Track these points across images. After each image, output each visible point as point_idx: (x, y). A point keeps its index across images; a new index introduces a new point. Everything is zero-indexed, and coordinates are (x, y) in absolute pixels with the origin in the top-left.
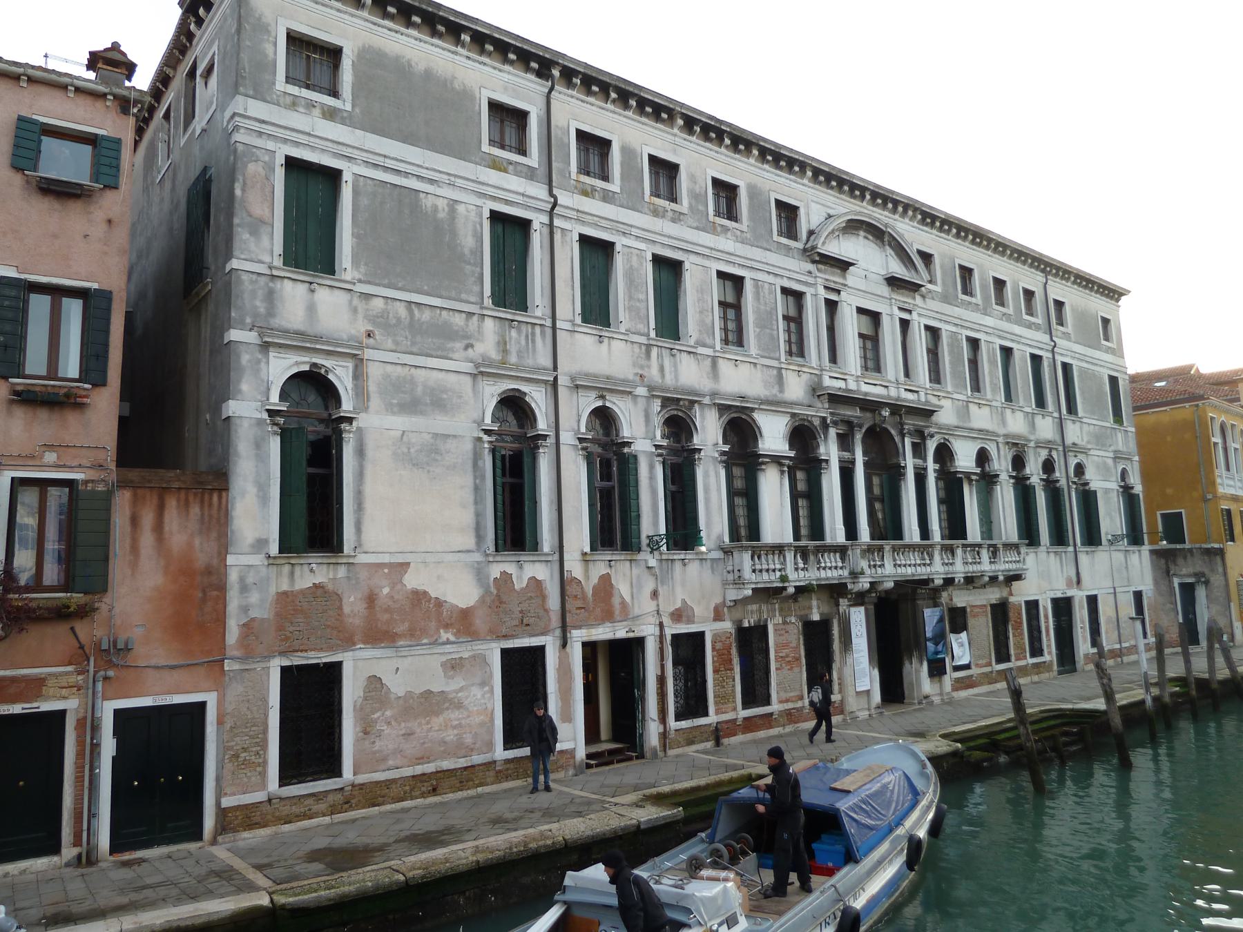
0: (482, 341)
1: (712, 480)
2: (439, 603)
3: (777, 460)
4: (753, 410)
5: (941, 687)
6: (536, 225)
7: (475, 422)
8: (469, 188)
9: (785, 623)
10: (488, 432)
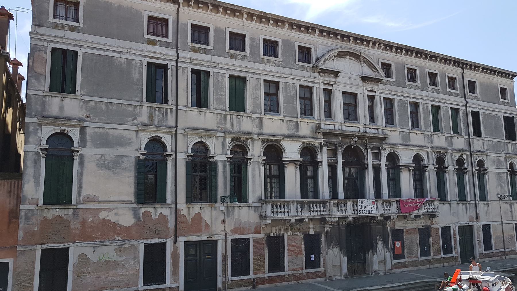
1: (257, 172)
6: (170, 67)
9: (294, 235)
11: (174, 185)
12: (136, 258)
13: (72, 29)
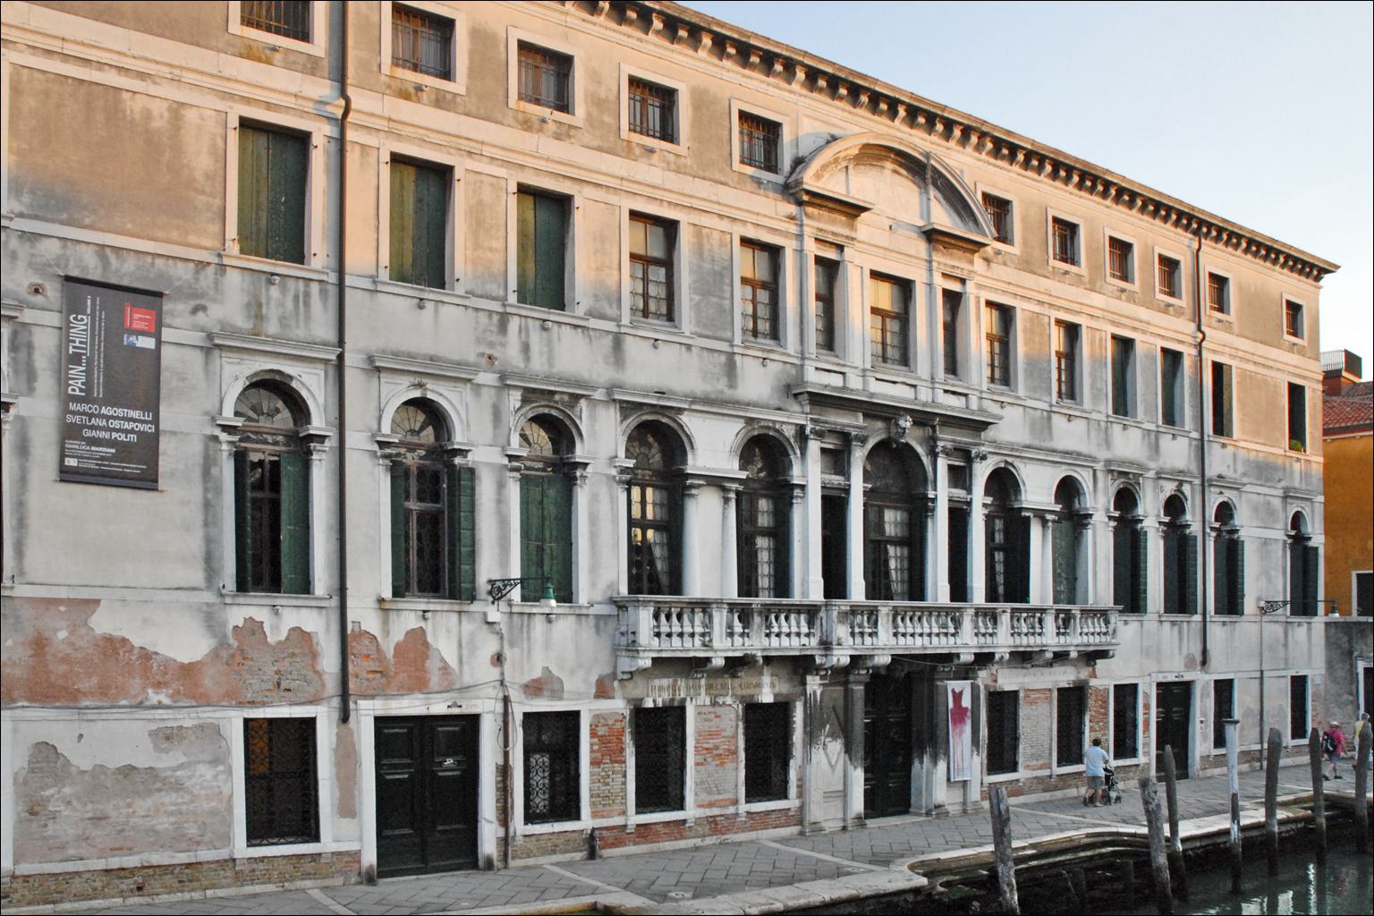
0: (222, 302)
2: (146, 656)
3: (717, 482)
4: (680, 411)
5: (965, 795)
6: (318, 140)
7: (207, 413)
9: (714, 704)
10: (225, 428)
11: (335, 536)
12: (219, 760)
13: (441, 101)
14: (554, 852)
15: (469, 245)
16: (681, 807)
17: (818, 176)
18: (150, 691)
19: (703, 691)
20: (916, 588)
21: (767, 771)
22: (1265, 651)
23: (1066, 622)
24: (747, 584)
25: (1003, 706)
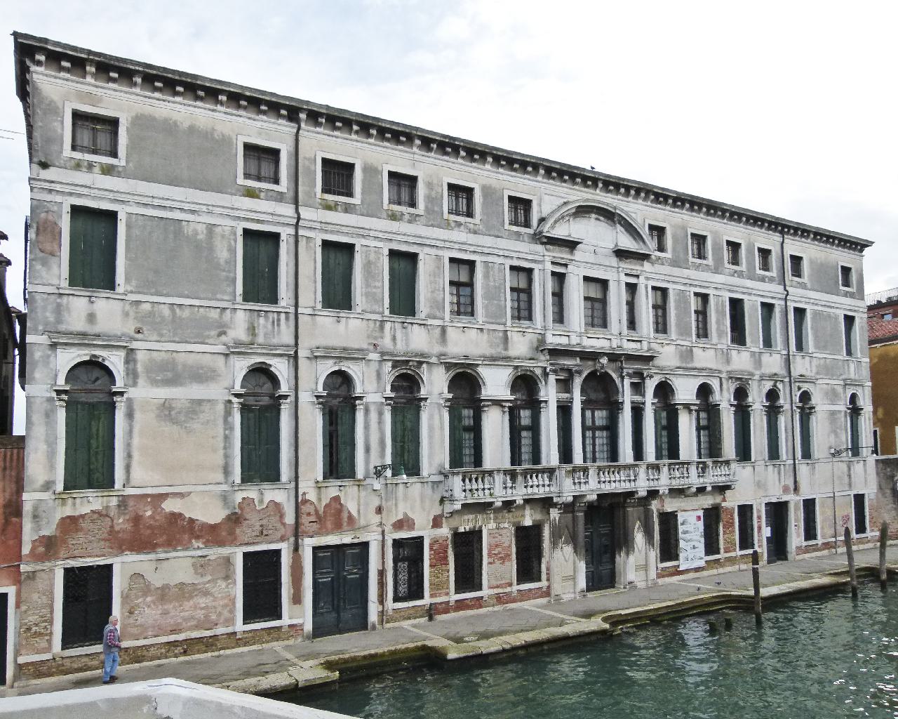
2: (192, 521)
3: (498, 403)
4: (478, 365)
6: (283, 237)
8: (226, 213)
10: (237, 396)
11: (293, 448)
13: (108, 170)
14: (409, 618)
15: (364, 286)
16: (480, 589)
17: (553, 227)
18: (193, 541)
19: (492, 521)
20: (613, 454)
21: (529, 565)
22: (835, 478)
23: (704, 470)
24: (515, 458)
25: (669, 521)
